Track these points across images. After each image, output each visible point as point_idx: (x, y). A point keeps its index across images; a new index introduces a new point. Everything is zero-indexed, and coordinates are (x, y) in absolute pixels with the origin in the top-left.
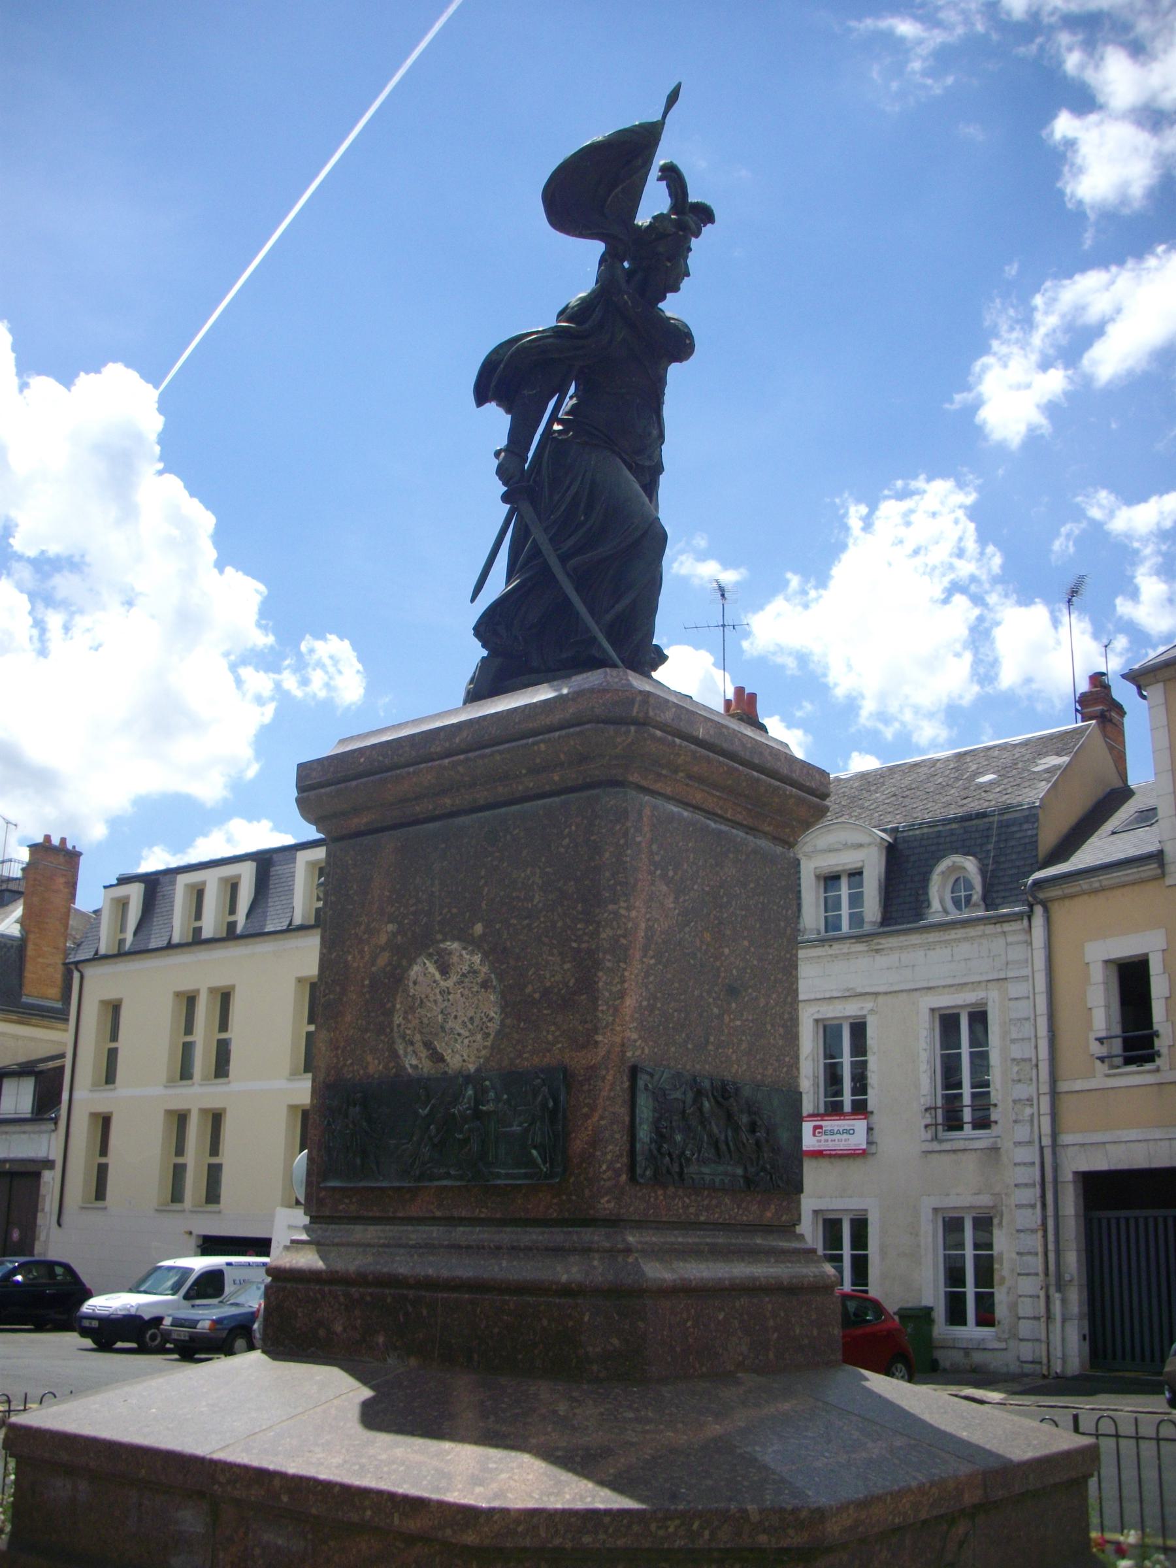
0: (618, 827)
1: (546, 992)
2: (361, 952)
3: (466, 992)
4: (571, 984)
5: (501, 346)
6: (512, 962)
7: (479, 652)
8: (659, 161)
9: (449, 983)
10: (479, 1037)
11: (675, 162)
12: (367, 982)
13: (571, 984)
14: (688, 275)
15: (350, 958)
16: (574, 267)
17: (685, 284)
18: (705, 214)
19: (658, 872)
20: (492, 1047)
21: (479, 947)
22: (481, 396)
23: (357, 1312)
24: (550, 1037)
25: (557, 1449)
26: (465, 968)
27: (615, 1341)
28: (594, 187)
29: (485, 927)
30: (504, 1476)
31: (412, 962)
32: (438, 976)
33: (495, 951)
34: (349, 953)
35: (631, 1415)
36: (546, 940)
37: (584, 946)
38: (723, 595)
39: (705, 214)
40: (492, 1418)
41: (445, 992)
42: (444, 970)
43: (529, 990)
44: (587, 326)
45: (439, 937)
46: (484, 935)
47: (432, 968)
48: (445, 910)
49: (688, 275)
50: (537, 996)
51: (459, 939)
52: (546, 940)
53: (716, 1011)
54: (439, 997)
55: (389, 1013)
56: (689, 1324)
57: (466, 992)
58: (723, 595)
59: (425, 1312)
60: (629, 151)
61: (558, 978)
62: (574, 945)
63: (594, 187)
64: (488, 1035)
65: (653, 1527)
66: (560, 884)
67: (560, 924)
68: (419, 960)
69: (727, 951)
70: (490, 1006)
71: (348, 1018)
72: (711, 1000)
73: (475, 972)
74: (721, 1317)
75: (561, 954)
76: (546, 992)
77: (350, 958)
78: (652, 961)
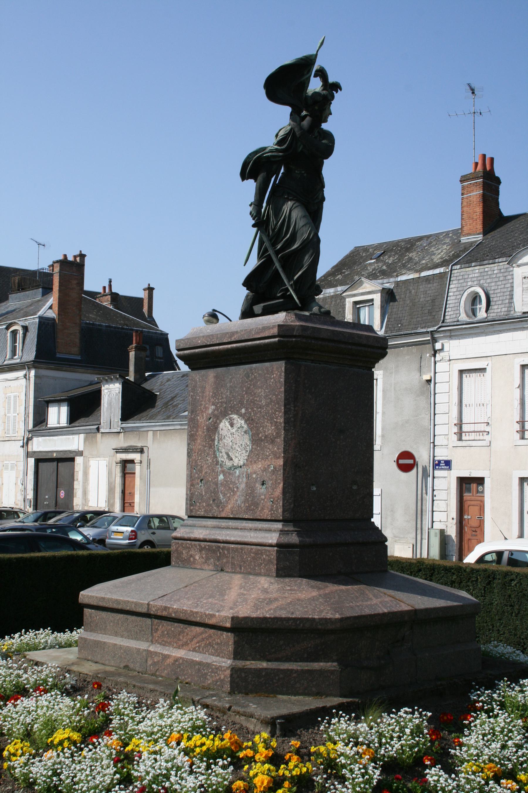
0: (290, 376)
1: (266, 437)
2: (203, 416)
3: (239, 434)
4: (274, 435)
5: (250, 154)
6: (255, 424)
7: (244, 292)
8: (316, 67)
9: (234, 431)
10: (244, 452)
11: (323, 66)
12: (205, 428)
13: (274, 435)
14: (331, 114)
15: (199, 418)
16: (271, 123)
17: (330, 118)
18: (336, 87)
19: (308, 391)
20: (248, 456)
21: (244, 418)
22: (244, 175)
23: (203, 552)
24: (268, 454)
25: (260, 599)
26: (239, 426)
27: (288, 563)
28: (288, 83)
29: (246, 410)
30: (240, 607)
31: (221, 421)
32: (230, 427)
33: (249, 420)
34: (198, 416)
35: (289, 588)
36: (266, 417)
37: (279, 420)
38: (473, 93)
39: (336, 87)
40: (243, 589)
41: (232, 434)
42: (232, 425)
43: (260, 435)
44: (282, 147)
45: (230, 412)
46: (245, 413)
47: (227, 424)
48: (232, 403)
49: (331, 114)
50: (263, 438)
51: (237, 414)
52: (266, 417)
53: (334, 440)
54: (230, 435)
55: (213, 440)
56: (317, 557)
57: (239, 434)
58: (473, 93)
59: (226, 552)
60: (303, 67)
61: (270, 432)
62: (275, 420)
63: (288, 83)
64: (247, 451)
65: (284, 622)
66: (270, 396)
67: (270, 412)
68: (223, 421)
69: (339, 416)
70: (246, 440)
71: (199, 441)
72: (331, 436)
73: (242, 427)
74: (331, 554)
75: (271, 423)
76: (266, 437)
77: (199, 418)
78: (305, 425)
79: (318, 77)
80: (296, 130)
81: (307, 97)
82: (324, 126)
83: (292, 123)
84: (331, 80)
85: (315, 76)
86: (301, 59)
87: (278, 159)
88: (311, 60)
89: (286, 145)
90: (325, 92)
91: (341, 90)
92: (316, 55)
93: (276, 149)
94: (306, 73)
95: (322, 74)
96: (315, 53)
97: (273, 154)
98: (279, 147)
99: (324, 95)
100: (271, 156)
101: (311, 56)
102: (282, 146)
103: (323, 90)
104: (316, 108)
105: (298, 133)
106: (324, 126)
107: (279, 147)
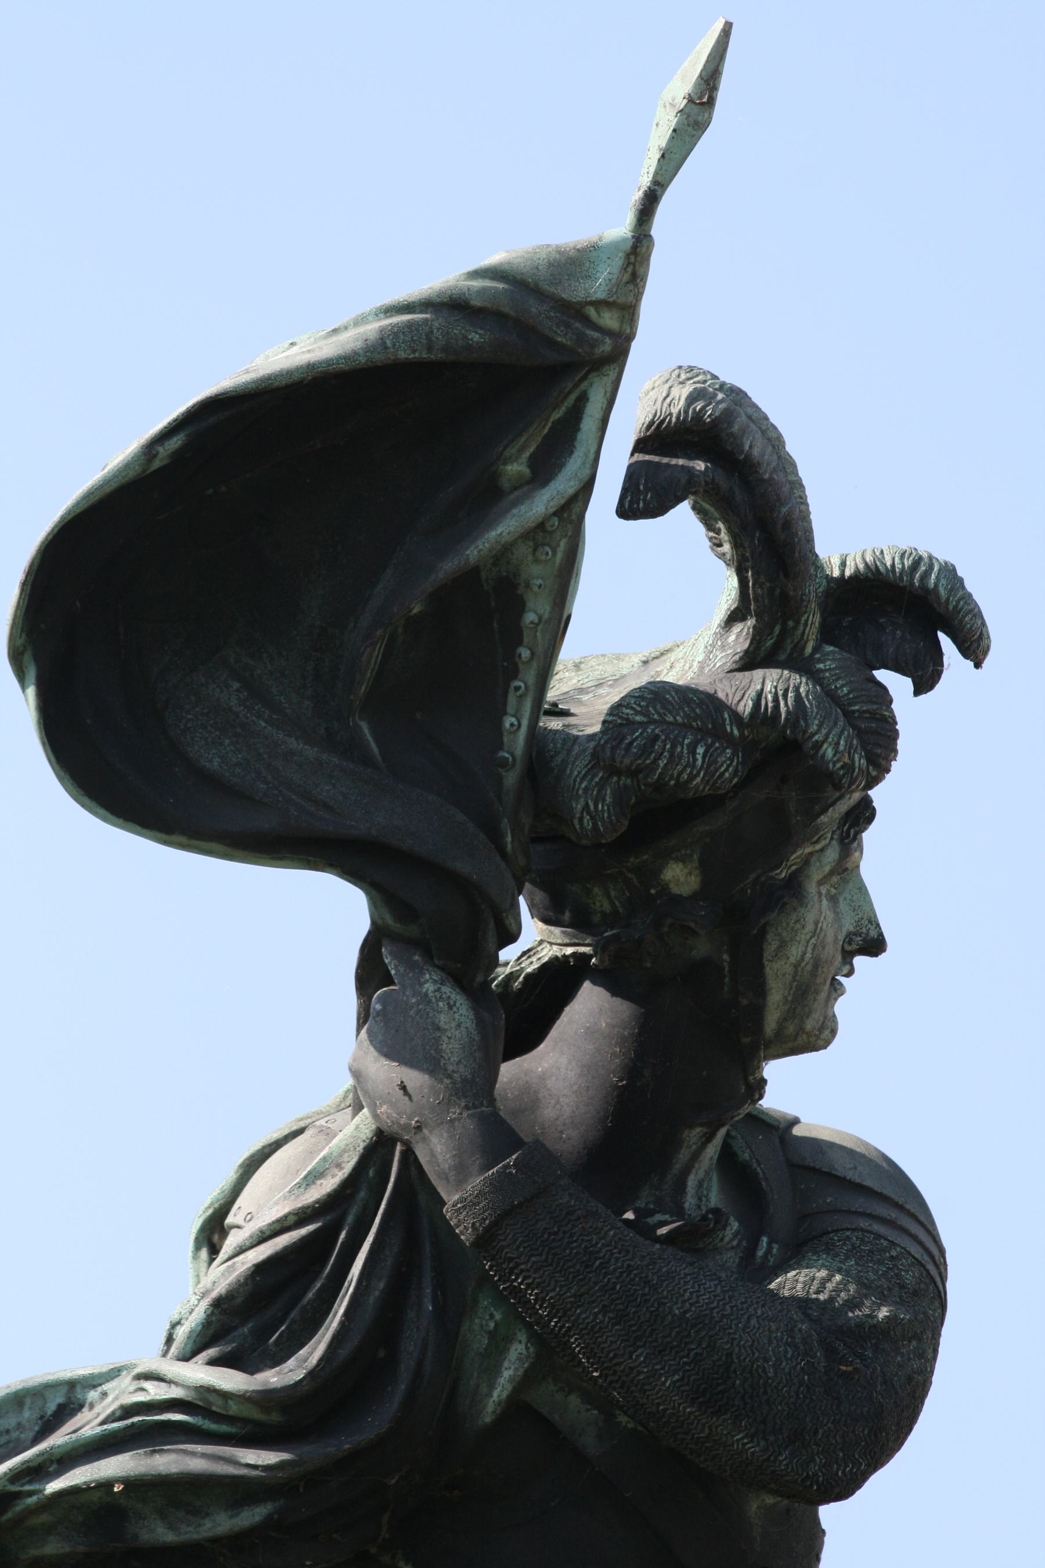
8: (641, 396)
14: (875, 946)
17: (864, 994)
18: (914, 617)
39: (914, 617)
44: (272, 1378)
49: (874, 945)
79: (683, 512)
80: (436, 1152)
81: (545, 756)
82: (793, 1089)
83: (385, 1072)
84: (844, 537)
85: (642, 500)
86: (451, 306)
87: (222, 1523)
88: (574, 312)
89: (314, 1352)
90: (769, 681)
91: (975, 648)
92: (637, 251)
93: (202, 1403)
94: (516, 468)
95: (722, 466)
96: (619, 227)
97: (167, 1462)
98: (230, 1380)
99: (762, 718)
100: (135, 1485)
101: (575, 262)
102: (276, 1359)
103: (750, 661)
104: (680, 876)
105: (461, 1197)
106: (793, 1089)
107: (230, 1380)
